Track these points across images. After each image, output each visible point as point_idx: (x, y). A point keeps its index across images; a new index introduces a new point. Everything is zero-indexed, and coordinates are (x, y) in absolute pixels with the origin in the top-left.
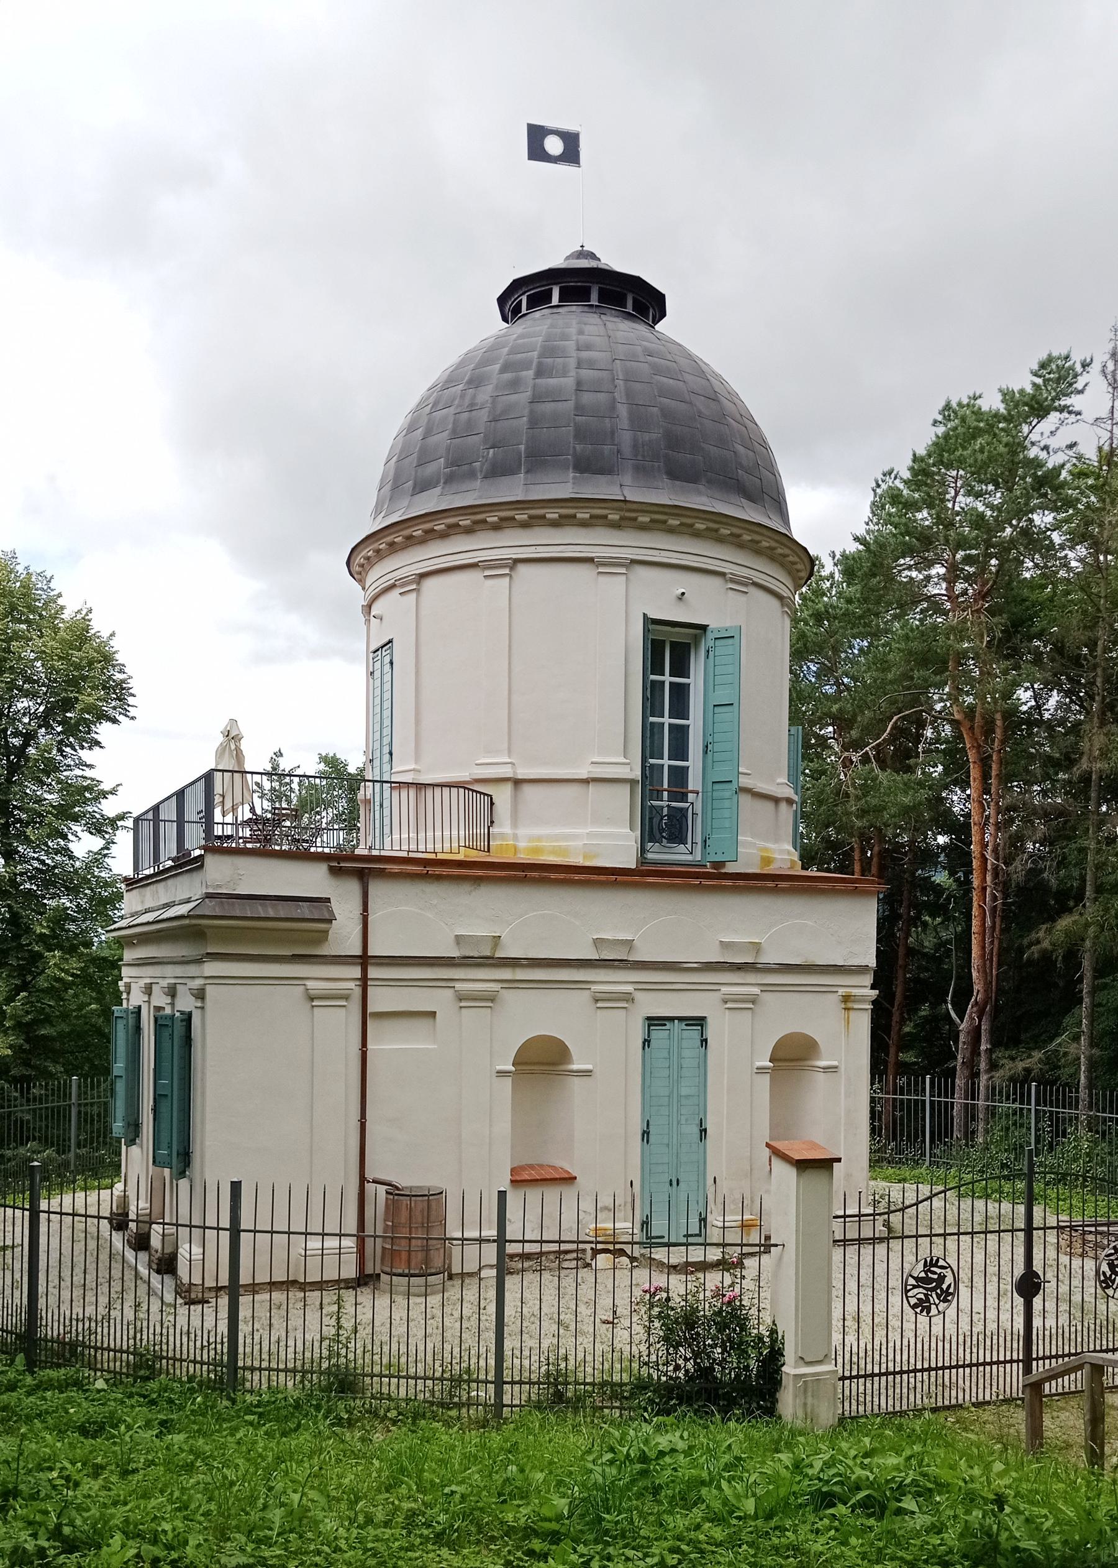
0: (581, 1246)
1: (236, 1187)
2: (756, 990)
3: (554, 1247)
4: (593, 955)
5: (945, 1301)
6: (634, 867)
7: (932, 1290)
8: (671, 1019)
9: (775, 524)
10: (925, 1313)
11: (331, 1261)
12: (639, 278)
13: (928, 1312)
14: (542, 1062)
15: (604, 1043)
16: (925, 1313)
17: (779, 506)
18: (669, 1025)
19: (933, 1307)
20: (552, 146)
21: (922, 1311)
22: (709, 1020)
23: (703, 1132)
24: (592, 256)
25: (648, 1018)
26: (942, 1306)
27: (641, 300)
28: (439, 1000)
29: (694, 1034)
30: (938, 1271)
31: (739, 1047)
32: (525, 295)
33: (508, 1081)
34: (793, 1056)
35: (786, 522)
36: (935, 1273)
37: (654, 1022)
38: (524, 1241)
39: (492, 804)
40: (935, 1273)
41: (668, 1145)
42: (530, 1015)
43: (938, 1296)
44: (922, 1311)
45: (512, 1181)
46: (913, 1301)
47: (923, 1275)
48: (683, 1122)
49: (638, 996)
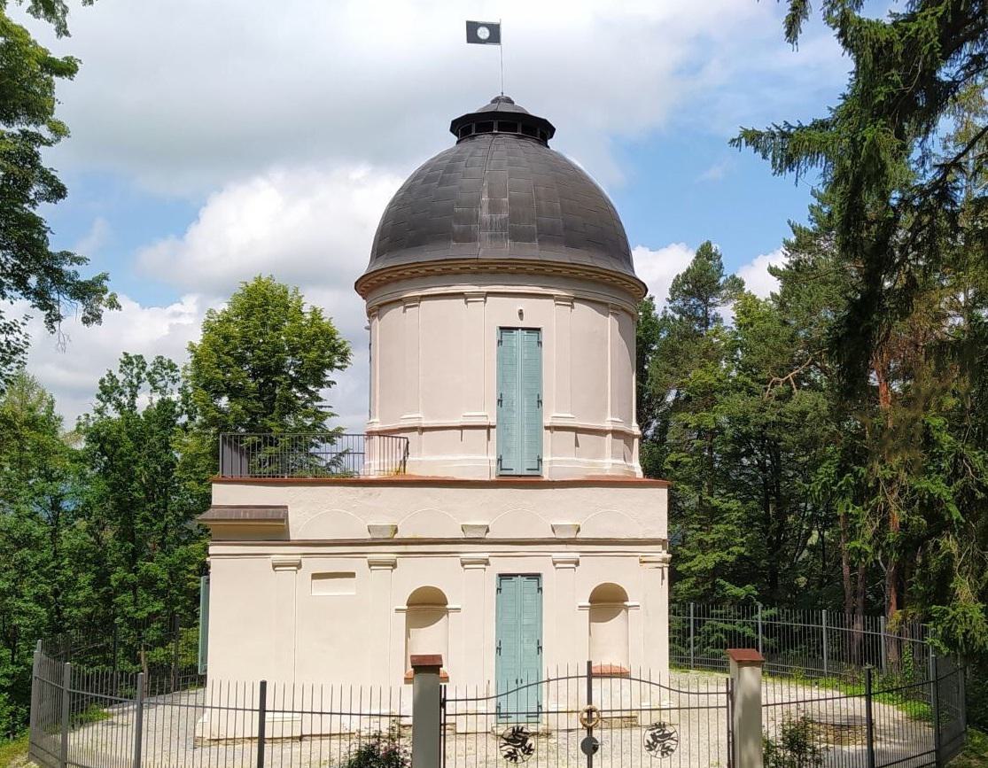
0: (634, 714)
1: (263, 685)
2: (578, 555)
3: (618, 714)
4: (461, 535)
5: (528, 754)
6: (666, 490)
7: (518, 747)
8: (516, 575)
9: (631, 274)
10: (513, 761)
11: (288, 725)
12: (545, 121)
13: (516, 760)
14: (427, 606)
15: (470, 591)
16: (513, 761)
17: (626, 257)
18: (514, 579)
19: (519, 758)
20: (482, 33)
21: (511, 760)
22: (544, 576)
23: (540, 648)
24: (509, 101)
25: (500, 575)
26: (526, 757)
27: (539, 130)
28: (358, 565)
29: (534, 583)
30: (523, 735)
31: (566, 592)
32: (466, 127)
33: (403, 615)
34: (607, 602)
35: (634, 272)
36: (520, 737)
37: (502, 576)
38: (621, 710)
39: (408, 443)
40: (520, 737)
41: (515, 657)
42: (418, 573)
43: (523, 751)
44: (511, 760)
45: (405, 679)
46: (506, 753)
47: (512, 737)
48: (525, 641)
49: (491, 560)
